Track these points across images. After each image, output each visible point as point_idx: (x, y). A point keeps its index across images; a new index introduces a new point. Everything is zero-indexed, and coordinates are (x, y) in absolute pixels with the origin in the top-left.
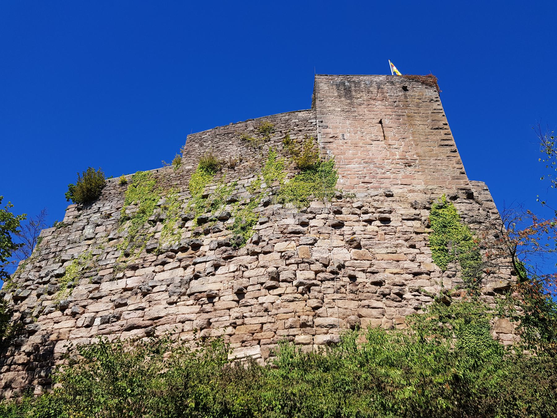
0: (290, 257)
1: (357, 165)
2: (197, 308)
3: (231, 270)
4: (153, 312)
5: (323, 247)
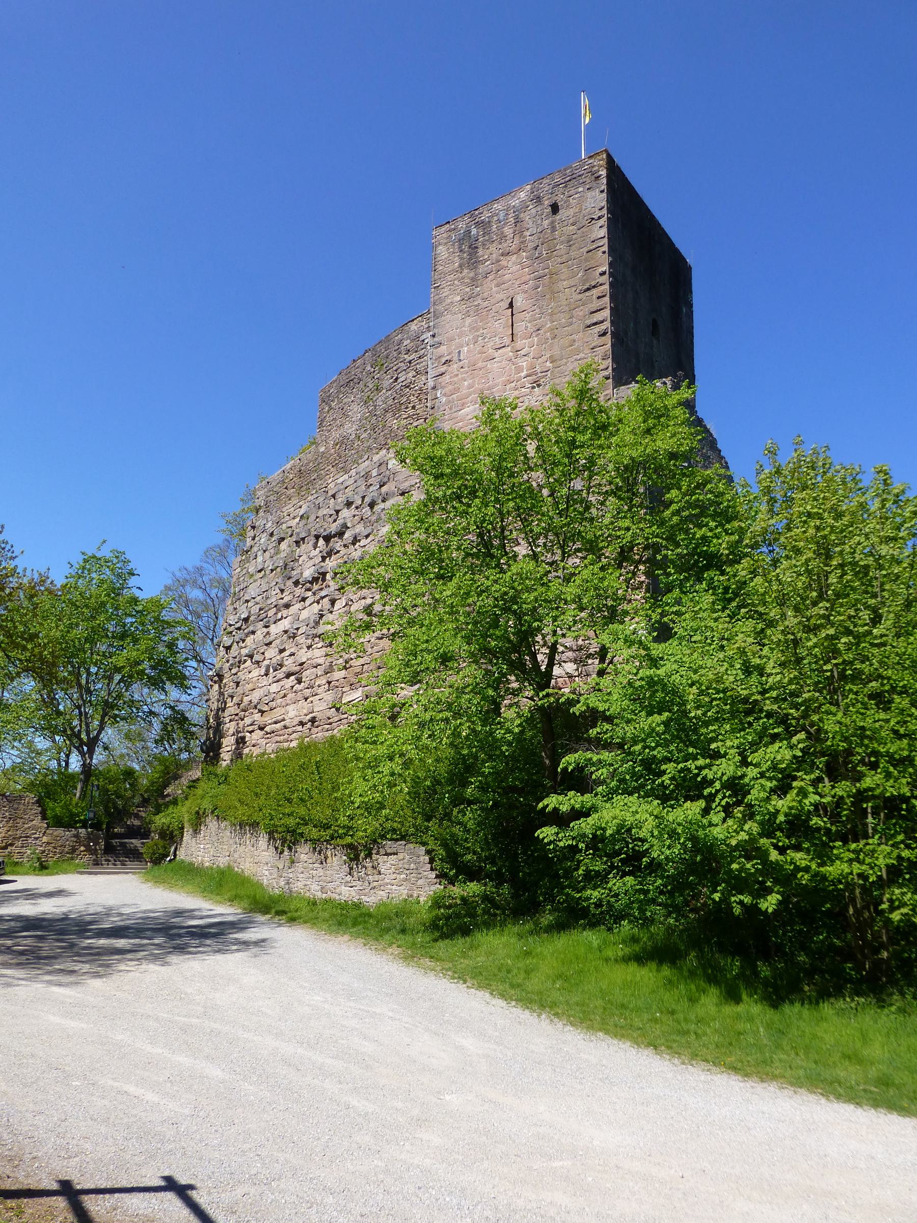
1: (472, 408)
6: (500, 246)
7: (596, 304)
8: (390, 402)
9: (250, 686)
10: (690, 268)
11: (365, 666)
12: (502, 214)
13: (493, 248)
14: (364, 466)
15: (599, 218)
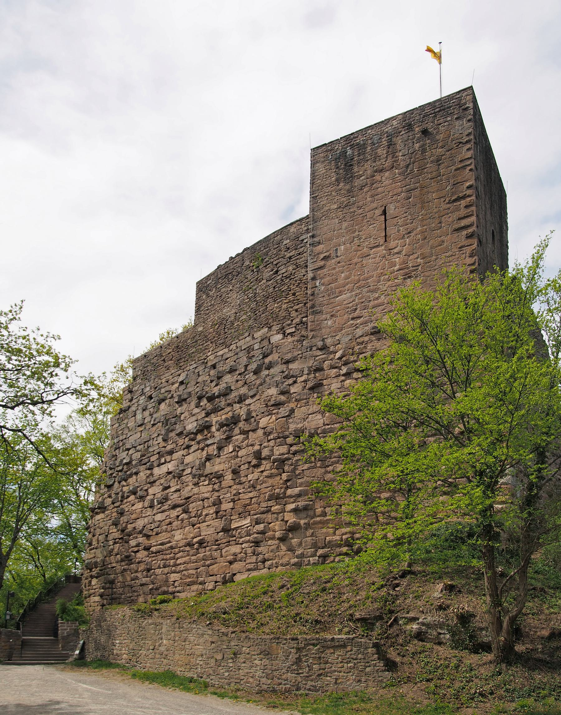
0: (270, 433)
1: (349, 295)
2: (210, 488)
3: (230, 451)
4: (186, 493)
5: (298, 417)
6: (374, 164)
7: (463, 212)
8: (271, 290)
9: (134, 516)
11: (253, 500)
12: (376, 138)
13: (367, 165)
14: (243, 343)
15: (467, 142)
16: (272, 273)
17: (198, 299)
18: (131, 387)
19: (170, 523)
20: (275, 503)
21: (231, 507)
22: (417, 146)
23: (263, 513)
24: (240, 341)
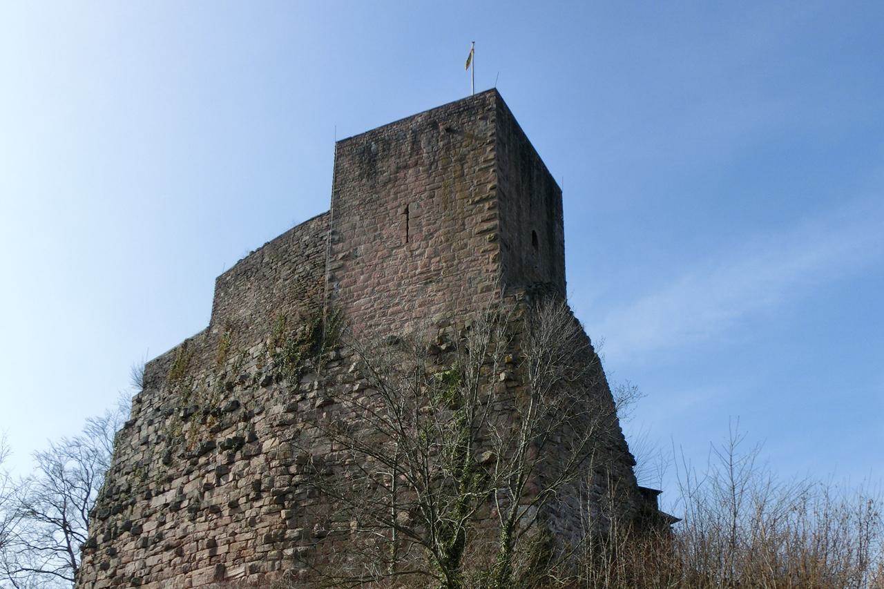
6: (398, 161)
10: (560, 192)
16: (289, 271)
17: (217, 296)
18: (140, 397)
19: (161, 570)
20: (272, 548)
21: (226, 551)
22: (441, 144)
23: (259, 559)
24: (252, 347)
